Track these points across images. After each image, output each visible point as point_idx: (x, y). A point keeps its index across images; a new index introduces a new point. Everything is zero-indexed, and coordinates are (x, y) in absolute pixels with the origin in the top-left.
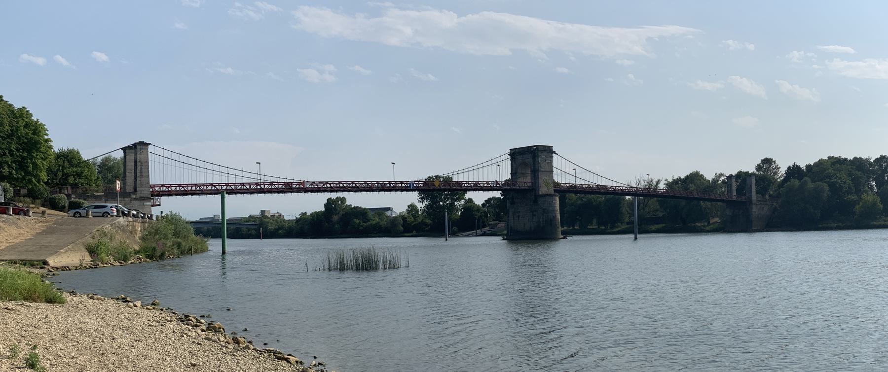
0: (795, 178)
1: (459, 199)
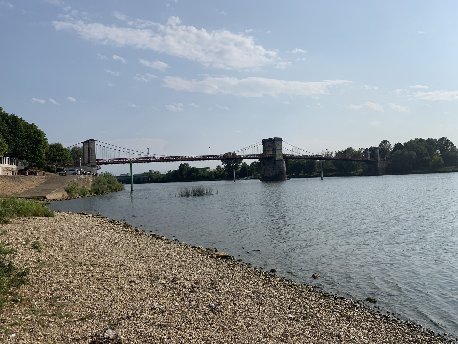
0: (398, 149)
1: (240, 163)
